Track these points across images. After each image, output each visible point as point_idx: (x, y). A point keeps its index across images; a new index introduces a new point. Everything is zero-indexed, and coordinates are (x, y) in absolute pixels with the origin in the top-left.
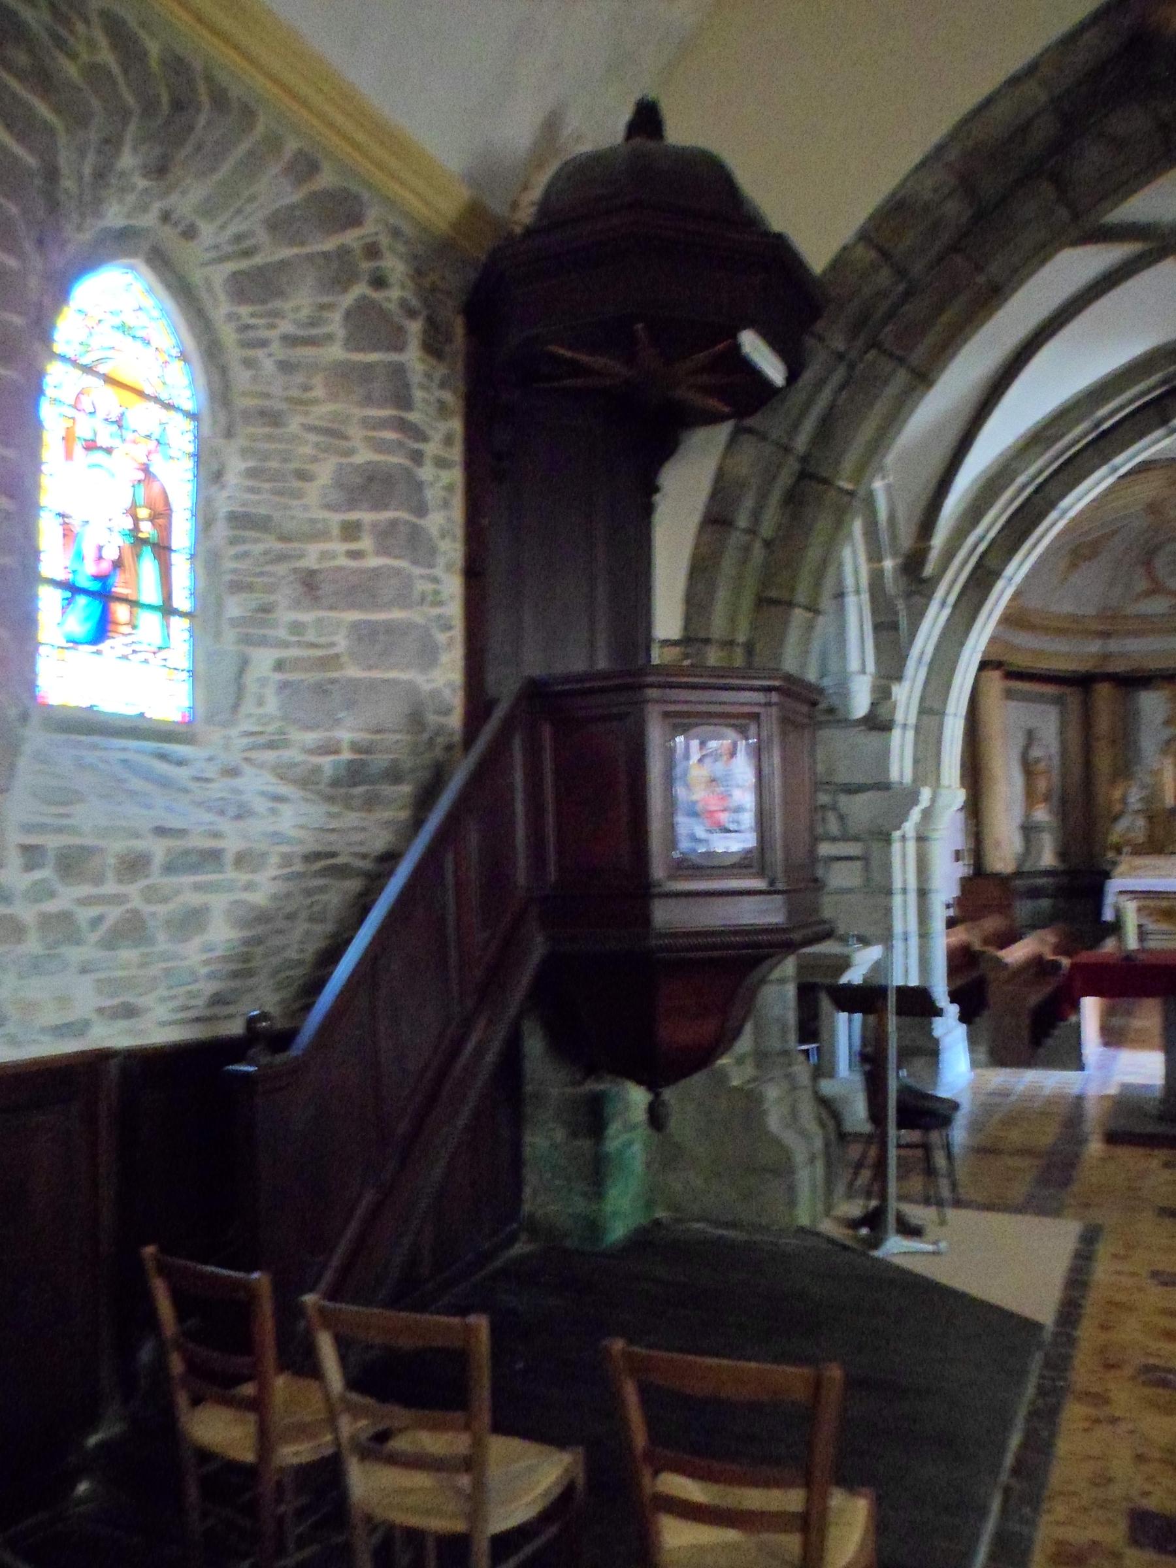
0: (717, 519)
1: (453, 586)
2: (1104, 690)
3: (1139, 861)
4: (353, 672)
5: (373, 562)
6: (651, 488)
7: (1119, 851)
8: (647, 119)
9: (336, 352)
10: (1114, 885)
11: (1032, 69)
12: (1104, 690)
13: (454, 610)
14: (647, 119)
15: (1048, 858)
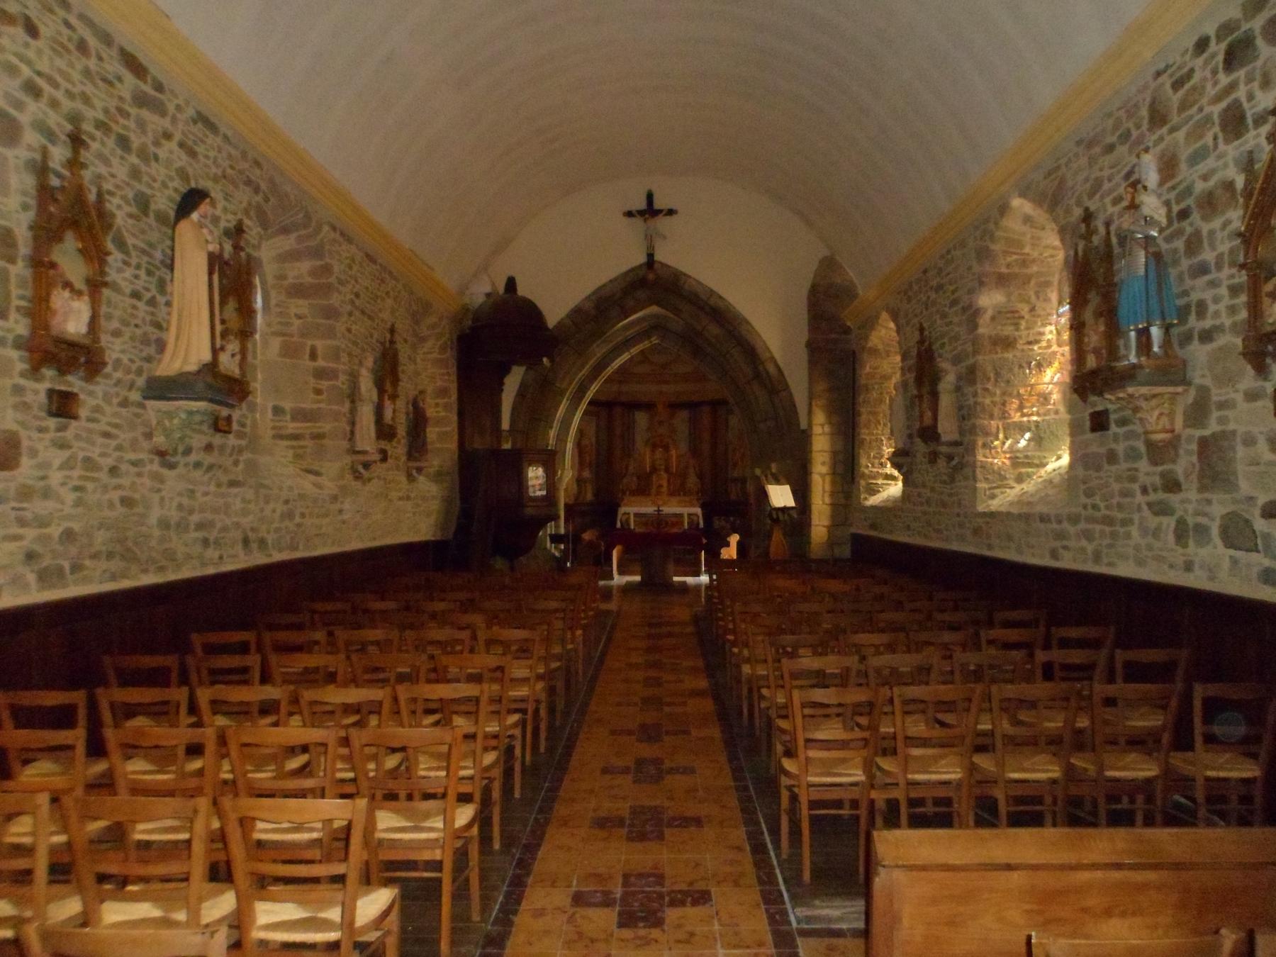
0: (521, 394)
1: (455, 418)
2: (618, 410)
3: (633, 499)
4: (438, 445)
5: (443, 414)
6: (502, 384)
7: (624, 493)
8: (511, 284)
9: (435, 355)
10: (622, 510)
11: (616, 279)
12: (618, 410)
13: (455, 425)
14: (511, 284)
15: (589, 496)
